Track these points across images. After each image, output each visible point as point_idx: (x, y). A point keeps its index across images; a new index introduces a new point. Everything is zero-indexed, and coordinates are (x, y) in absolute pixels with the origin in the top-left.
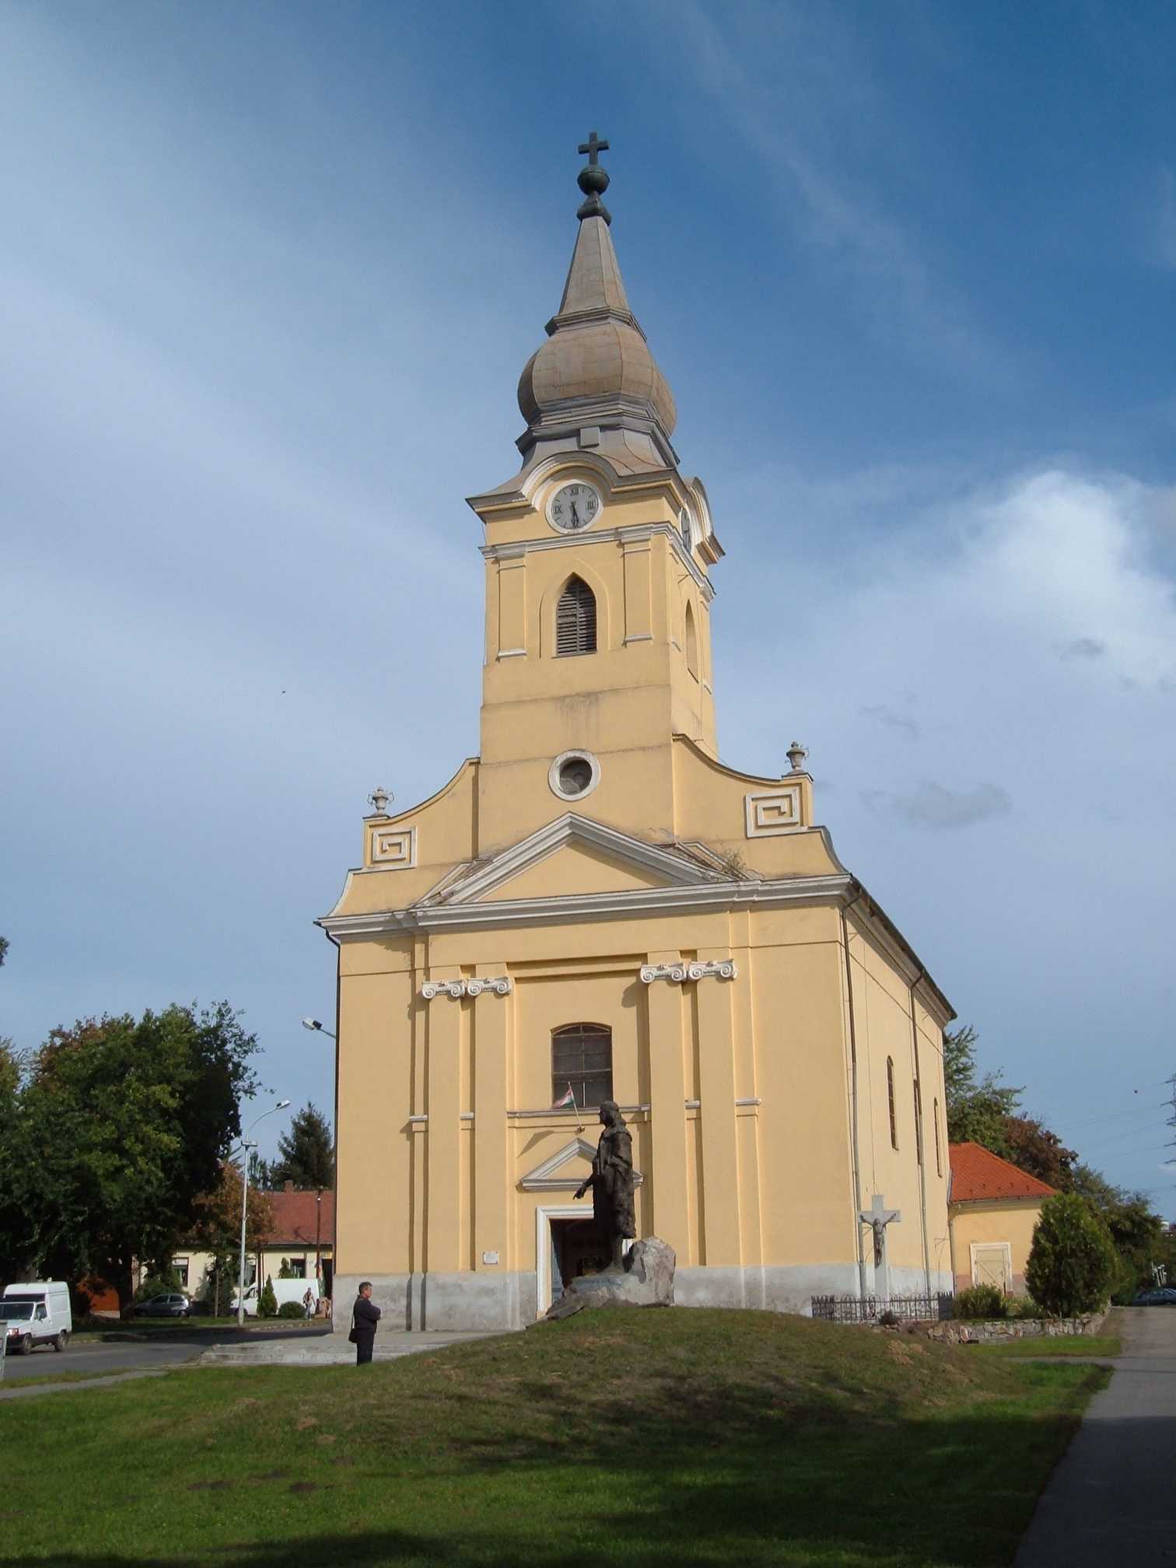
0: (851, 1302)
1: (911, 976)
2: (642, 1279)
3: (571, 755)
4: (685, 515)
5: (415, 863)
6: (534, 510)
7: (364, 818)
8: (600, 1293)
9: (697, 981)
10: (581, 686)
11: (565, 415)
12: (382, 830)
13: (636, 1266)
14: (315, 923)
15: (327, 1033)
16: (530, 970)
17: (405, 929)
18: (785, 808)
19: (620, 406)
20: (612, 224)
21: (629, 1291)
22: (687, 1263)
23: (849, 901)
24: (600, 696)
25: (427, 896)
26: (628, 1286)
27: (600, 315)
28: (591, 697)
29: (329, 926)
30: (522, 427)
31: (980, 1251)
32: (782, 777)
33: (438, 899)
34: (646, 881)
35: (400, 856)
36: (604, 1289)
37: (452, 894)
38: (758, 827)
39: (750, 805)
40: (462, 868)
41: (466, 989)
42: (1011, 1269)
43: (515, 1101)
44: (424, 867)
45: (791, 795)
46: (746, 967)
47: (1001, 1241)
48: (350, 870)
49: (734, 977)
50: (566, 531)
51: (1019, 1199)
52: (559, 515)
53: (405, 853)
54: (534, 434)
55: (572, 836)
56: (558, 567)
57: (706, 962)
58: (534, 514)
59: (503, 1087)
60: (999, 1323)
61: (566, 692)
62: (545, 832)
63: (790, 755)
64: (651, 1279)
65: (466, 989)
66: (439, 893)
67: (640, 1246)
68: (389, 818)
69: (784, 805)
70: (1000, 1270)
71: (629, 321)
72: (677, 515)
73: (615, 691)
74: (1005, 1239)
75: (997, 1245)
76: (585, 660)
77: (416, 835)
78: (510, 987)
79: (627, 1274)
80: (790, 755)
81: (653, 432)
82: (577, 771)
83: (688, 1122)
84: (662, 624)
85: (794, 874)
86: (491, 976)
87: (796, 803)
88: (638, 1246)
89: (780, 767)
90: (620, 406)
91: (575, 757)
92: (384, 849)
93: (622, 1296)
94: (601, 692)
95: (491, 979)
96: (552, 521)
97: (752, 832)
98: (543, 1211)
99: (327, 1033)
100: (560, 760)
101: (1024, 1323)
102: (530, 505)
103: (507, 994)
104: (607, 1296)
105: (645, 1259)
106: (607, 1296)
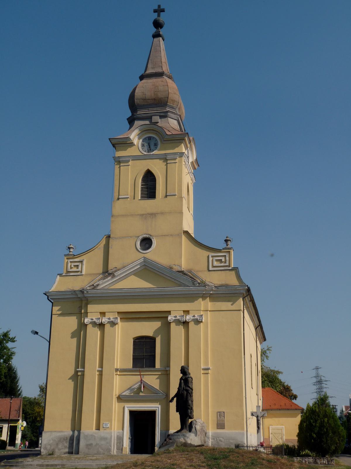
0: (244, 447)
1: (256, 324)
2: (196, 435)
3: (145, 236)
4: (188, 150)
5: (84, 273)
6: (135, 145)
7: (64, 255)
8: (181, 440)
9: (189, 322)
10: (149, 211)
11: (147, 111)
12: (71, 260)
13: (193, 429)
14: (44, 293)
15: (41, 336)
16: (127, 316)
17: (79, 297)
18: (223, 260)
19: (167, 109)
20: (164, 41)
21: (191, 439)
22: (211, 431)
23: (245, 296)
24: (156, 215)
25: (89, 285)
26: (191, 438)
27: (160, 75)
28: (153, 215)
29: (49, 295)
30: (129, 114)
31: (273, 429)
32: (223, 248)
33: (92, 287)
34: (150, 283)
35: (78, 270)
36: (182, 438)
37: (98, 285)
38: (213, 267)
39: (211, 259)
40: (101, 276)
41: (102, 321)
42: (284, 437)
43: (118, 364)
44: (86, 275)
45: (226, 256)
46: (208, 318)
47: (281, 426)
48: (58, 274)
49: (203, 321)
50: (146, 153)
51: (288, 410)
52: (143, 147)
53: (80, 269)
54: (135, 117)
55: (144, 266)
56: (142, 167)
57: (193, 315)
58: (134, 146)
59: (114, 359)
60: (299, 458)
61: (143, 213)
62: (132, 265)
63: (226, 241)
64: (199, 435)
65: (102, 321)
66: (93, 285)
67: (194, 422)
68: (74, 256)
69: (223, 259)
70: (280, 437)
71: (170, 77)
72: (186, 150)
73: (162, 213)
74: (282, 425)
75: (280, 427)
76: (150, 202)
77: (85, 262)
78: (118, 321)
79: (191, 433)
80: (226, 241)
81: (178, 119)
82: (147, 243)
83: (203, 375)
84: (180, 190)
85: (226, 284)
86: (112, 317)
87: (227, 258)
88: (194, 421)
89: (221, 245)
90: (167, 109)
91: (146, 237)
92: (72, 267)
93: (189, 442)
94: (157, 214)
95: (111, 318)
96: (141, 149)
97: (211, 268)
98: (127, 407)
99: (41, 336)
100: (141, 238)
101: (309, 458)
102: (133, 143)
103: (117, 324)
104: (183, 441)
105: (196, 427)
106: (183, 441)
